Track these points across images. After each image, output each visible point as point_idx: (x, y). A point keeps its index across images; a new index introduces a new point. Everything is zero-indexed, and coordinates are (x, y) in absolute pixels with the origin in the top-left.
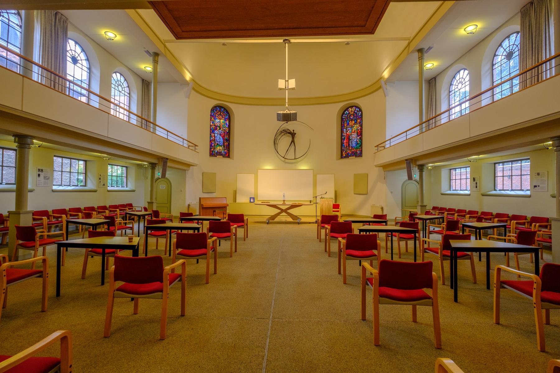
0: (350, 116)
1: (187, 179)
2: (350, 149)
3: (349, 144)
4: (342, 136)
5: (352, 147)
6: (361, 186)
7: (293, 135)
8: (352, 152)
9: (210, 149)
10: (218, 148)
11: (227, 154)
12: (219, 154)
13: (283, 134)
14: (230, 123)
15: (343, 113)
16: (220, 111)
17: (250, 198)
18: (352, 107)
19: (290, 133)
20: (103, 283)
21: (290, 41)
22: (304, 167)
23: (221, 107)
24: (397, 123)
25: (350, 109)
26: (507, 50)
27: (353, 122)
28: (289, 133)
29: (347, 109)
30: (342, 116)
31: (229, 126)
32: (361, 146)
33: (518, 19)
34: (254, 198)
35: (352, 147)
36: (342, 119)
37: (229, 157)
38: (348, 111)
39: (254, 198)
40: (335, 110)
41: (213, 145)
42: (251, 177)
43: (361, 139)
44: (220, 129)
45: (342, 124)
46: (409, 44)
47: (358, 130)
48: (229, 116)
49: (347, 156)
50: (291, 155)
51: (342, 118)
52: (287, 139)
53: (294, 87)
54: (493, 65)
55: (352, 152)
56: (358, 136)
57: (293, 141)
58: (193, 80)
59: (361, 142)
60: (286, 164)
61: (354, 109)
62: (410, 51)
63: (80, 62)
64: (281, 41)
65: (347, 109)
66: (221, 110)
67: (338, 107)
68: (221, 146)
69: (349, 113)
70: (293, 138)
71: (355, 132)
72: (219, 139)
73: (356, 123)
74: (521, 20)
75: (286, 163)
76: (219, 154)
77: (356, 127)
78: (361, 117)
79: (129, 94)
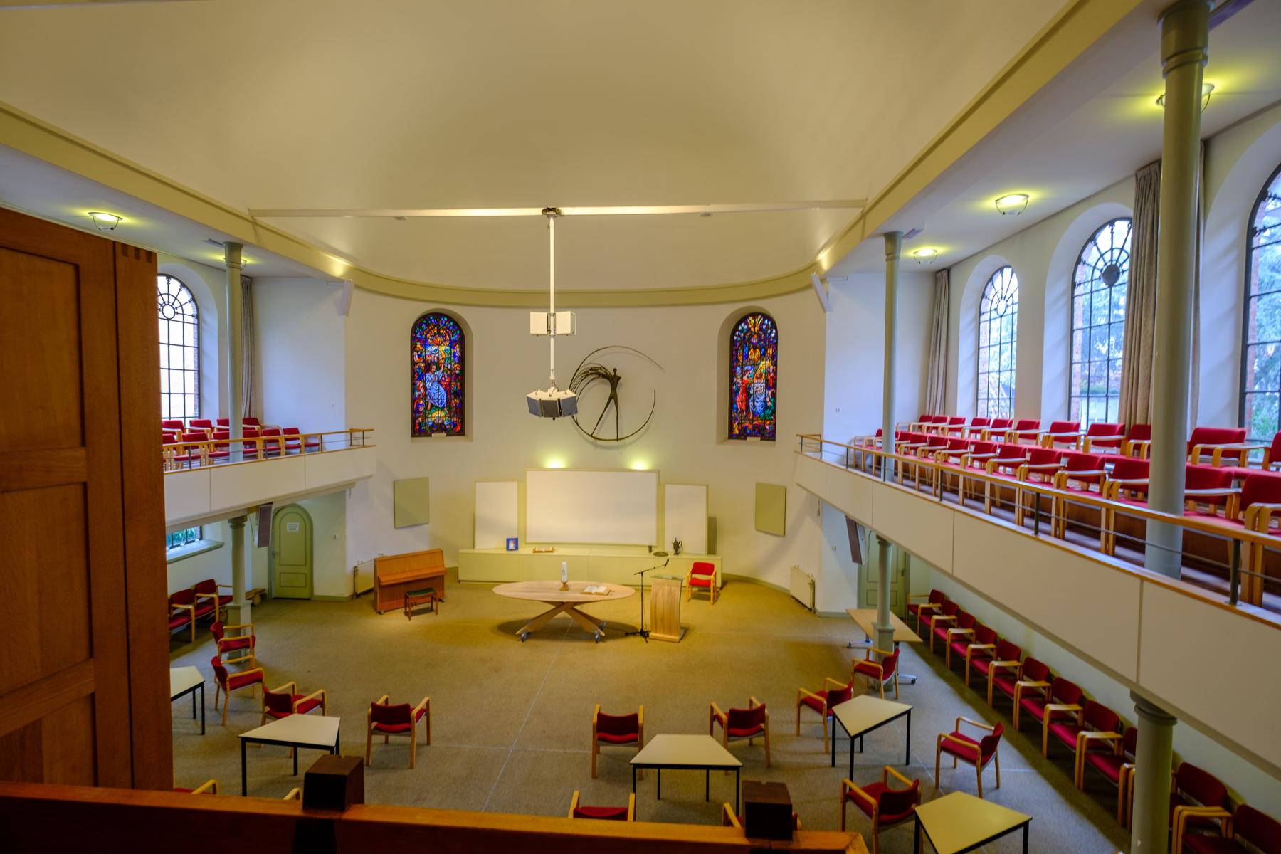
0: (751, 337)
2: (749, 420)
3: (747, 406)
4: (732, 383)
5: (754, 414)
6: (771, 506)
7: (614, 380)
9: (414, 420)
10: (435, 415)
11: (458, 428)
12: (439, 427)
13: (591, 377)
14: (463, 351)
15: (736, 329)
16: (437, 325)
17: (508, 540)
18: (755, 315)
19: (606, 376)
21: (558, 213)
22: (640, 462)
23: (438, 315)
24: (850, 389)
25: (751, 321)
26: (1107, 257)
27: (758, 352)
29: (744, 320)
31: (462, 360)
32: (774, 413)
33: (1130, 191)
34: (516, 541)
35: (754, 414)
36: (733, 343)
37: (462, 432)
38: (746, 323)
39: (516, 541)
40: (715, 320)
41: (422, 409)
42: (509, 490)
43: (774, 395)
44: (438, 368)
46: (863, 216)
47: (767, 373)
48: (462, 336)
49: (743, 435)
50: (607, 431)
53: (569, 331)
54: (1074, 285)
56: (768, 388)
57: (613, 396)
58: (356, 271)
59: (775, 404)
61: (759, 320)
62: (869, 231)
64: (538, 211)
65: (744, 320)
66: (437, 325)
67: (721, 315)
68: (442, 409)
69: (749, 329)
70: (614, 388)
72: (438, 393)
73: (763, 356)
74: (1137, 201)
75: (597, 446)
76: (439, 427)
77: (764, 365)
78: (774, 344)
79: (198, 316)
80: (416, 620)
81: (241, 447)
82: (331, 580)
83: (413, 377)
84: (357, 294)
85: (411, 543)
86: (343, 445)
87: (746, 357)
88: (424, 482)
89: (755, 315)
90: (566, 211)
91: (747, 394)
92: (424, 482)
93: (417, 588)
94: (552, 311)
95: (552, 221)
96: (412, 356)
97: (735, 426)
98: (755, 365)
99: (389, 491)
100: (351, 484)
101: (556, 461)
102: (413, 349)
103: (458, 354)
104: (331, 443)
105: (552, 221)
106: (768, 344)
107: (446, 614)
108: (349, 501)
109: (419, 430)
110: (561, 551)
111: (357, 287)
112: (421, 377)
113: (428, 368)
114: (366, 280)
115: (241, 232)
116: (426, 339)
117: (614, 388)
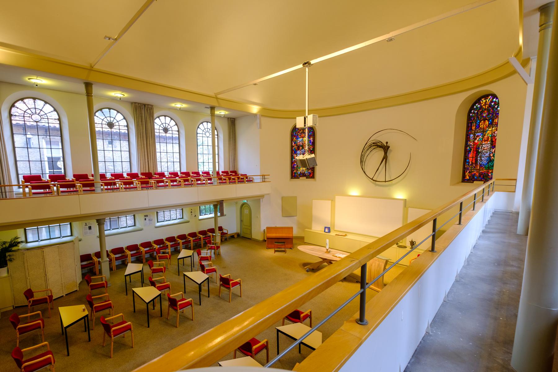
1: (261, 208)
3: (476, 160)
4: (466, 145)
5: (481, 166)
7: (385, 148)
8: (481, 174)
13: (374, 147)
17: (325, 227)
18: (486, 97)
20: (461, 204)
22: (400, 194)
27: (487, 123)
28: (380, 147)
30: (470, 112)
35: (481, 166)
38: (480, 103)
39: (329, 228)
41: (295, 166)
42: (327, 204)
45: (468, 126)
49: (472, 180)
51: (469, 115)
52: (379, 154)
55: (481, 174)
57: (385, 158)
60: (377, 187)
63: (170, 129)
64: (301, 66)
65: (478, 101)
69: (481, 107)
70: (386, 153)
71: (487, 140)
76: (303, 175)
79: (178, 131)
80: (277, 254)
81: (216, 179)
82: (258, 233)
83: (292, 153)
84: (264, 120)
85: (281, 222)
86: (259, 181)
87: (478, 127)
88: (295, 198)
89: (486, 97)
90: (312, 62)
91: (477, 152)
92: (295, 198)
93: (282, 241)
94: (307, 115)
95: (307, 69)
96: (292, 144)
97: (467, 174)
98: (484, 131)
99: (280, 201)
100: (262, 196)
101: (355, 191)
102: (292, 140)
103: (312, 141)
104: (257, 179)
105: (307, 69)
106: (493, 114)
107: (289, 254)
108: (262, 204)
109: (294, 176)
110: (349, 237)
111: (262, 116)
112: (296, 153)
113: (298, 149)
114: (268, 113)
115: (214, 103)
116: (298, 135)
117: (386, 153)
